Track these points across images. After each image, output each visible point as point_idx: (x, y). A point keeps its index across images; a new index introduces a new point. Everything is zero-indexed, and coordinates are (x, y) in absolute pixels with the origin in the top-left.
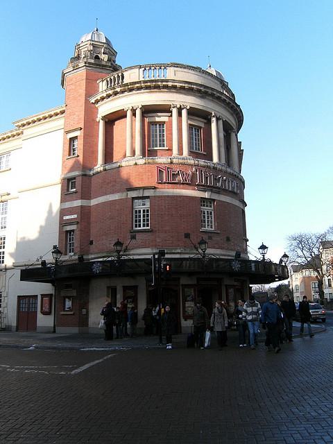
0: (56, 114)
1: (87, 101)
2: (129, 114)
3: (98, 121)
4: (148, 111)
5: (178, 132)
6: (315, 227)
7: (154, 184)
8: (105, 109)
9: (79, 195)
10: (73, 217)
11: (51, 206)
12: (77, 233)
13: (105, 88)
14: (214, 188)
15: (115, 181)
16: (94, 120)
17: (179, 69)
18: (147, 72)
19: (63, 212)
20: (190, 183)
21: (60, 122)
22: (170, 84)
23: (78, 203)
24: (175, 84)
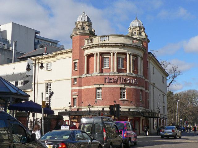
0: (69, 52)
1: (80, 49)
2: (95, 55)
3: (84, 56)
4: (102, 54)
5: (112, 62)
6: (194, 87)
7: (103, 83)
8: (87, 52)
9: (78, 85)
10: (76, 93)
11: (59, 42)
12: (77, 99)
13: (87, 42)
14: (126, 83)
15: (90, 81)
16: (83, 56)
17: (114, 37)
18: (102, 38)
19: (72, 91)
20: (116, 83)
21: (71, 54)
22: (110, 44)
23: (77, 88)
24: (112, 44)
